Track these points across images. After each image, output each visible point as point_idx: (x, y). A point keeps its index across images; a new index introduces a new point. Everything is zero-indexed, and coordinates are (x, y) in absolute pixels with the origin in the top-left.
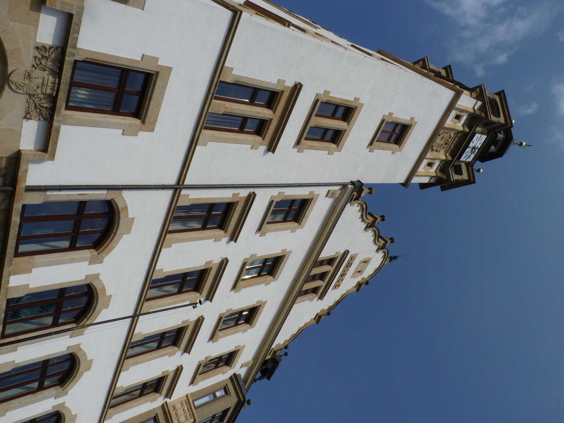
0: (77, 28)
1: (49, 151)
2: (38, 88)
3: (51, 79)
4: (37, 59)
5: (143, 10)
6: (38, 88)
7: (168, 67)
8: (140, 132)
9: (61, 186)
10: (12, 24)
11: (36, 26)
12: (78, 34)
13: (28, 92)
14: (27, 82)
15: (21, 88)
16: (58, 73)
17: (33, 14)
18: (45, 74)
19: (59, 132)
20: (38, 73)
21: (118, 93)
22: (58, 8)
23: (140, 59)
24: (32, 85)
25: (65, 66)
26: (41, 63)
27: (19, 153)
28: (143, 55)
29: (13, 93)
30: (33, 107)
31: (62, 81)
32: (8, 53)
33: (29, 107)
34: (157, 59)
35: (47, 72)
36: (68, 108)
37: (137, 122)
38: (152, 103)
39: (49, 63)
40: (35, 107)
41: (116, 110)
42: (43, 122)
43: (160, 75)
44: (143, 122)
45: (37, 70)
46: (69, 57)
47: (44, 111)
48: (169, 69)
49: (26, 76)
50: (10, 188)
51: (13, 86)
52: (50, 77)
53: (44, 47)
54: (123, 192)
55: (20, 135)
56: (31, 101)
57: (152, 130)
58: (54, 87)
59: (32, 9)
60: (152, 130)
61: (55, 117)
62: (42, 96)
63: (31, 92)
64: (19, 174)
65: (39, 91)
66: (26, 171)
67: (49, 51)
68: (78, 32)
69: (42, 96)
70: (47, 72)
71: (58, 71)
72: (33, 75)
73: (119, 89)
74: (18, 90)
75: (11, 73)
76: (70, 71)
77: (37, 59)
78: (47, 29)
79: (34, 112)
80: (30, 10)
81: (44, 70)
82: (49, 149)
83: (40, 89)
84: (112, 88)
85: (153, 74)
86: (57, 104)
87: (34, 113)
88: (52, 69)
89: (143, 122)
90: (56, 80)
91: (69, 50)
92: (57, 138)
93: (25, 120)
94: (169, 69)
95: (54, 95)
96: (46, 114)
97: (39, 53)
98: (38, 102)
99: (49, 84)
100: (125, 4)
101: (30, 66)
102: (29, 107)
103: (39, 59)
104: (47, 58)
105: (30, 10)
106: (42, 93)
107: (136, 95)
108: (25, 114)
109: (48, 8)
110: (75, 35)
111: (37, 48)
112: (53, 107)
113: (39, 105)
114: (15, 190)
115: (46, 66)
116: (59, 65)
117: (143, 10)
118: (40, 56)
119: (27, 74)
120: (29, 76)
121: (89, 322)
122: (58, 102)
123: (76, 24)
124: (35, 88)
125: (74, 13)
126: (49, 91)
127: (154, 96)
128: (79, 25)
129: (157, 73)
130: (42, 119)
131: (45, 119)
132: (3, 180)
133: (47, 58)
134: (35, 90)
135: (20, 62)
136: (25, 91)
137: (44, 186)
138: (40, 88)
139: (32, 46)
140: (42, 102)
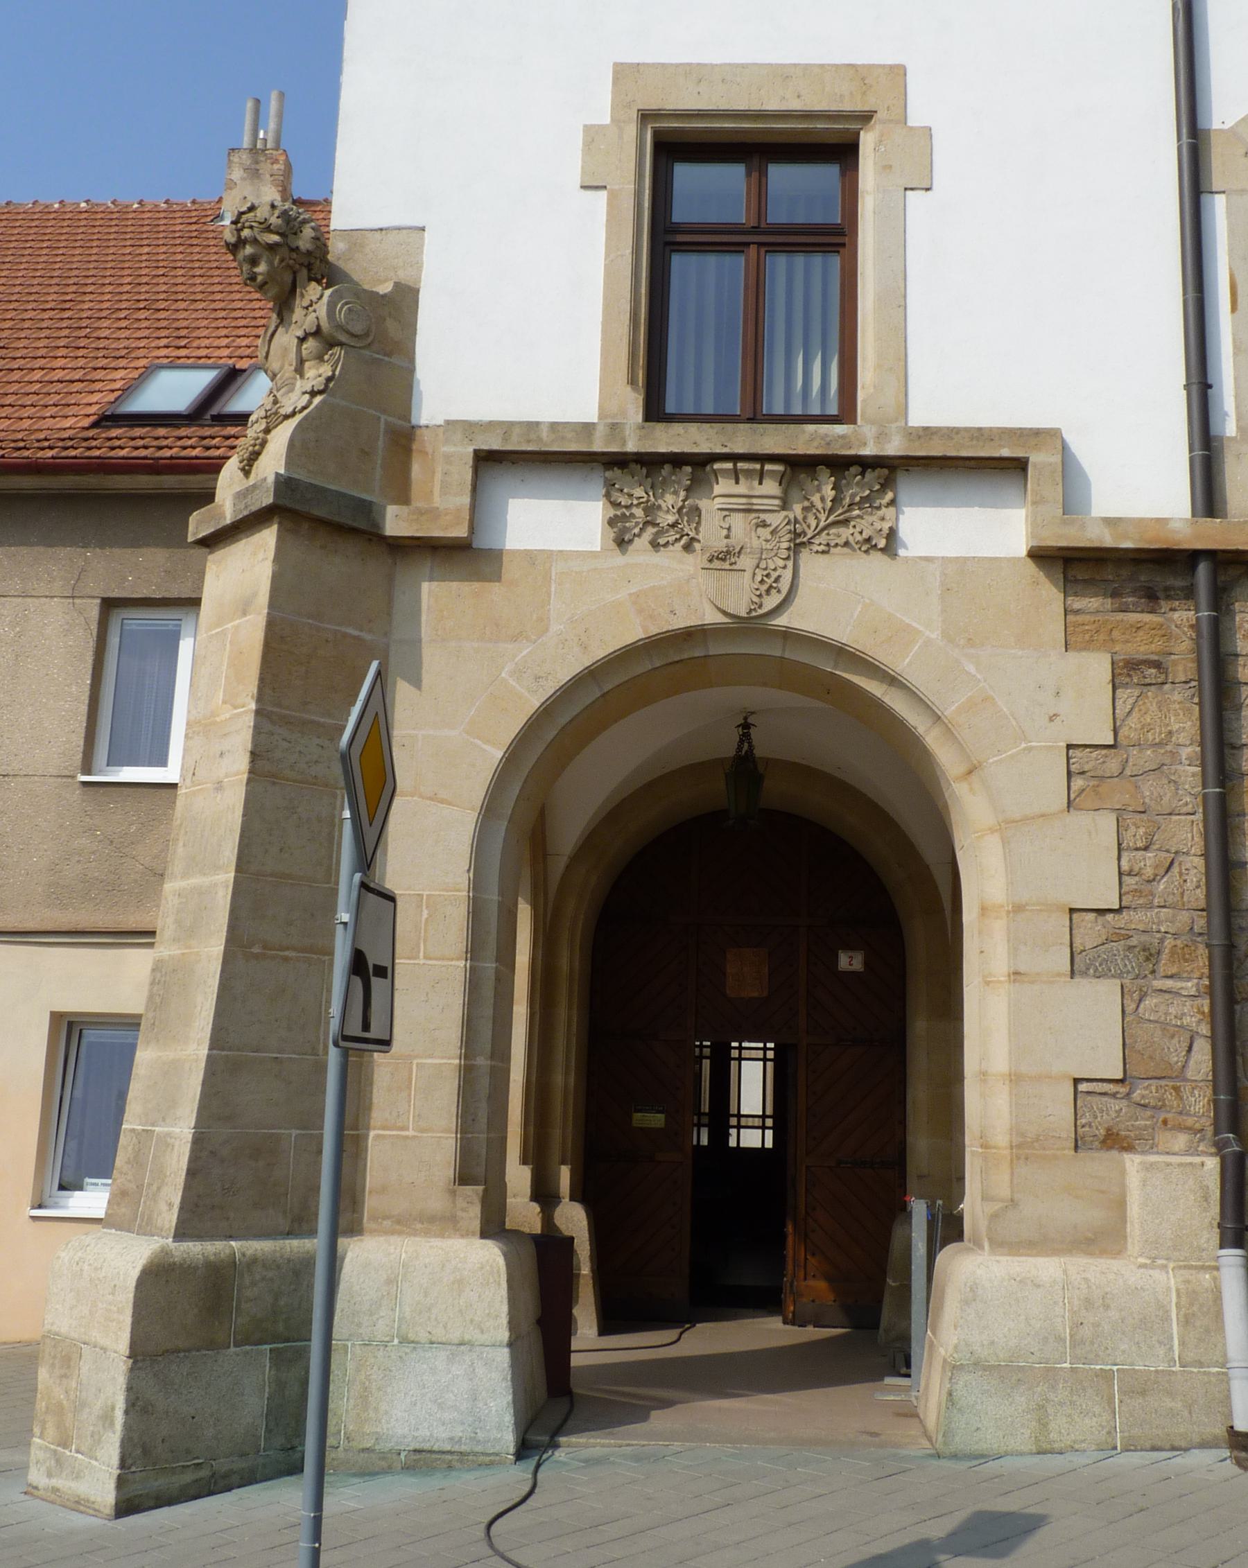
0: (517, 430)
1: (1019, 453)
2: (764, 525)
3: (723, 486)
4: (662, 541)
5: (423, 229)
6: (764, 525)
7: (616, 80)
8: (912, 122)
10: (555, 627)
11: (549, 555)
12: (538, 423)
13: (784, 554)
14: (746, 562)
15: (774, 575)
16: (699, 466)
17: (510, 570)
18: (709, 506)
19: (926, 429)
20: (711, 533)
21: (760, 244)
22: (466, 500)
23: (603, 195)
24: (756, 543)
25: (662, 449)
26: (673, 526)
27: (1039, 556)
28: (583, 187)
29: (798, 601)
30: (845, 533)
31: (719, 450)
32: (654, 630)
33: (846, 544)
34: (592, 134)
35: (703, 504)
36: (847, 413)
37: (867, 141)
38: (773, 105)
40: (845, 522)
41: (834, 238)
42: (906, 487)
43: (653, 104)
44: (866, 117)
45: (700, 537)
46: (624, 443)
48: (624, 73)
49: (726, 566)
50: (1203, 569)
51: (771, 602)
52: (718, 489)
53: (611, 522)
54: (1216, 125)
55: (965, 560)
56: (823, 538)
57: (898, 73)
58: (749, 473)
59: (496, 577)
60: (898, 73)
61: (867, 451)
63: (785, 545)
64: (1128, 544)
65: (775, 519)
66: (1110, 522)
68: (533, 426)
69: (797, 509)
70: (703, 504)
71: (689, 469)
72: (721, 545)
73: (748, 244)
75: (725, 613)
76: (678, 428)
77: (662, 541)
78: (552, 524)
80: (499, 579)
81: (697, 511)
82: (1005, 452)
84: (843, 268)
85: (657, 133)
86: (812, 451)
87: (869, 524)
89: (866, 117)
90: (725, 472)
91: (598, 446)
92: (957, 431)
93: (902, 552)
94: (624, 73)
95: (779, 468)
96: (861, 485)
97: (639, 535)
98: (823, 517)
99: (742, 488)
100: (418, 291)
101: (689, 558)
102: (846, 544)
103: (657, 535)
104: (650, 509)
105: (499, 579)
106: (785, 506)
107: (763, 174)
108: (876, 557)
109: (472, 529)
110: (544, 434)
111: (622, 543)
112: (828, 466)
113: (831, 511)
114: (1211, 554)
115: (680, 510)
116: (667, 467)
117: (423, 229)
118: (651, 530)
119: (717, 564)
120: (725, 557)
122: (801, 451)
123: (506, 436)
124: (765, 533)
125: (471, 449)
126: (771, 487)
127: (741, 105)
128: (507, 427)
129: (645, 117)
131: (887, 484)
132: (1168, 597)
133: (650, 509)
135: (672, 589)
136: (781, 563)
137: (1191, 450)
138: (763, 516)
139: (618, 559)
140: (819, 505)
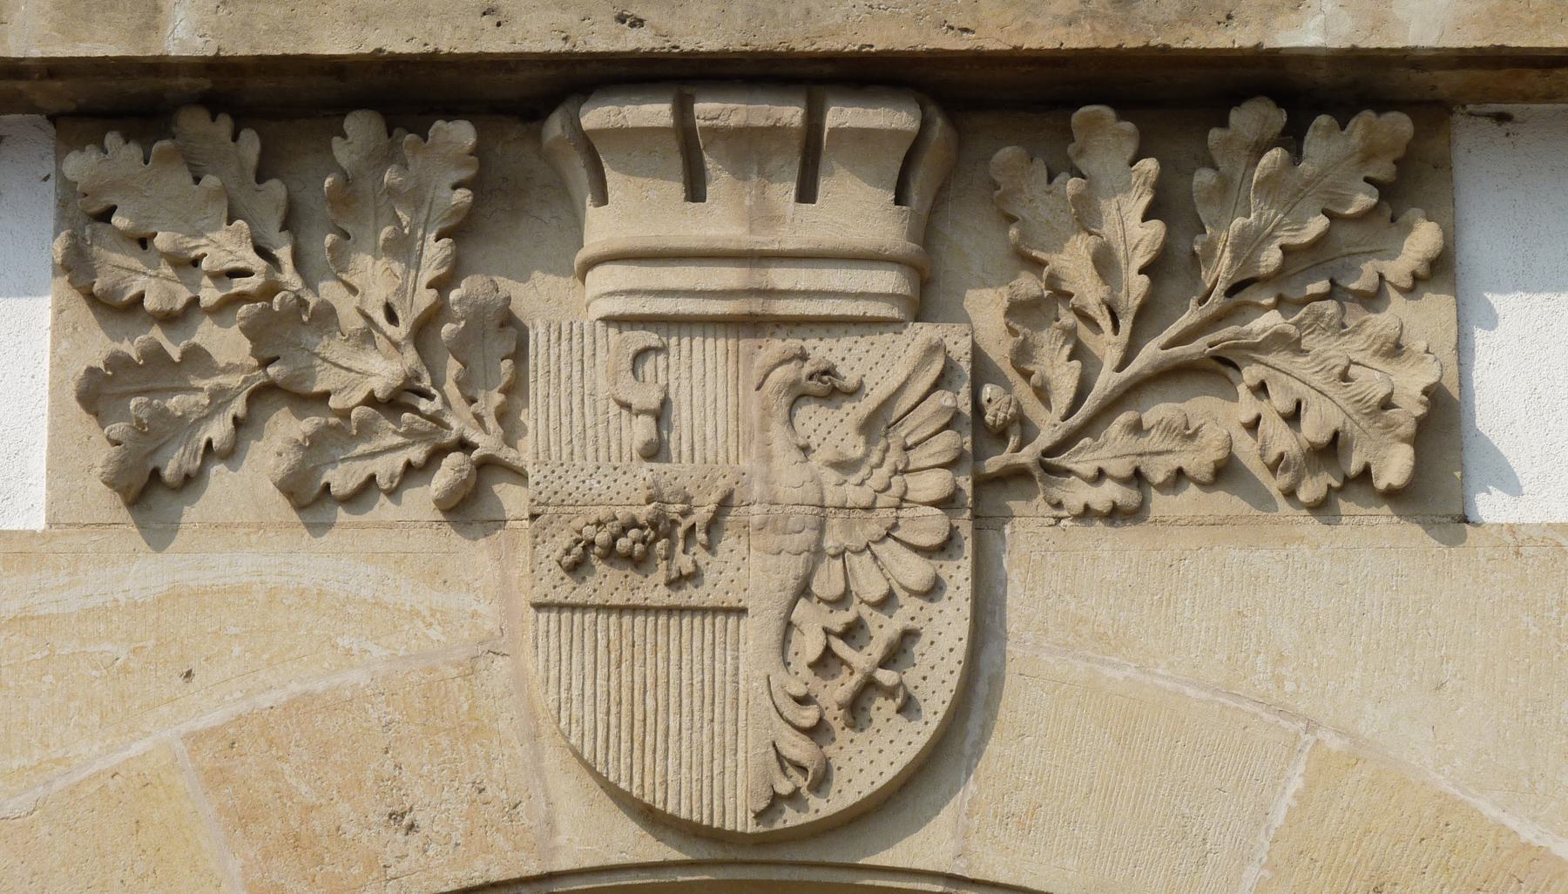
2: (830, 389)
3: (631, 210)
6: (830, 389)
9: (686, 250)
13: (929, 527)
14: (747, 570)
15: (883, 630)
18: (569, 310)
20: (576, 434)
26: (393, 404)
30: (1218, 419)
33: (1226, 472)
35: (538, 297)
39: (374, 280)
40: (1218, 369)
45: (524, 454)
47: (1258, 220)
49: (653, 588)
51: (871, 759)
52: (602, 227)
53: (97, 393)
56: (1113, 448)
58: (748, 147)
62: (986, 311)
63: (933, 484)
67: (170, 319)
69: (986, 311)
70: (538, 297)
71: (462, 134)
72: (626, 490)
74: (935, 675)
75: (651, 817)
79: (1293, 377)
83: (848, 356)
87: (1330, 374)
88: (460, 231)
93: (1490, 506)
95: (893, 118)
97: (230, 454)
99: (718, 220)
101: (475, 557)
102: (1226, 472)
103: (317, 447)
104: (282, 328)
106: (926, 298)
108: (1372, 532)
111: (149, 490)
112: (1125, 106)
113: (1148, 316)
115: (423, 331)
118: (286, 429)
119: (607, 583)
120: (646, 548)
121: (551, 72)
124: (832, 429)
126: (856, 210)
130: (1423, 239)
131: (1407, 186)
134: (872, 426)
136: (915, 571)
138: (823, 349)
139: (134, 570)
140: (1088, 290)
